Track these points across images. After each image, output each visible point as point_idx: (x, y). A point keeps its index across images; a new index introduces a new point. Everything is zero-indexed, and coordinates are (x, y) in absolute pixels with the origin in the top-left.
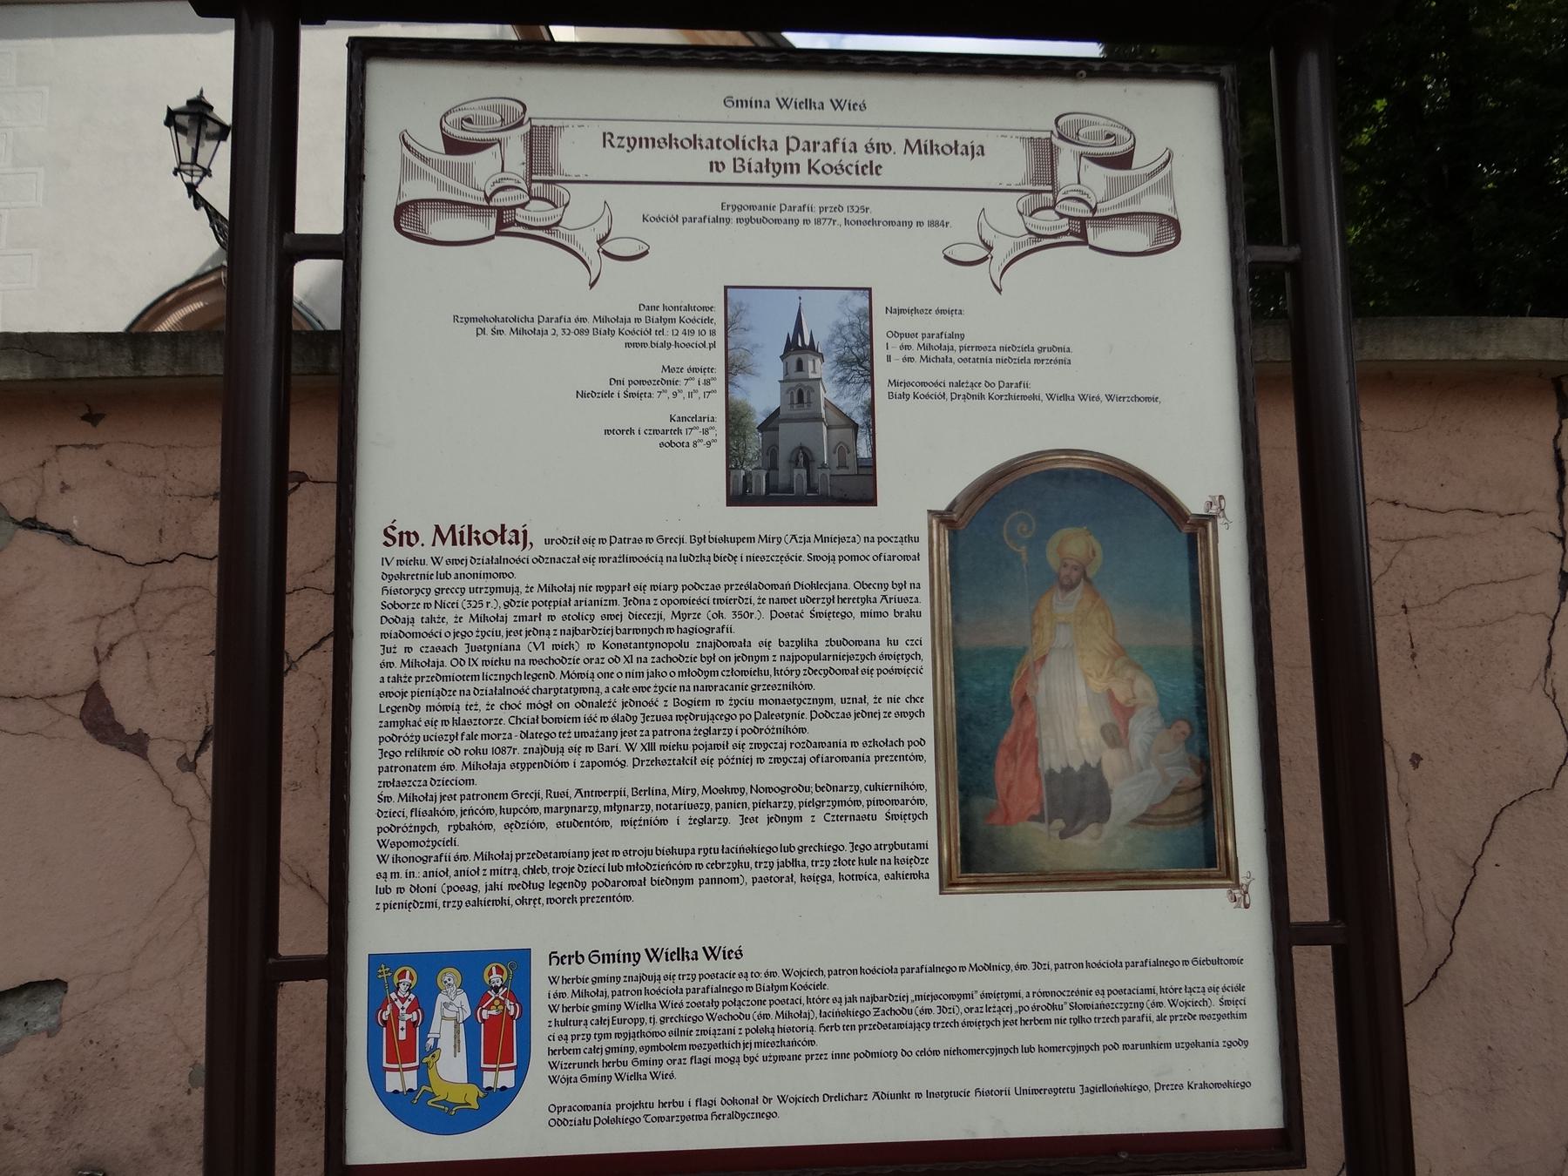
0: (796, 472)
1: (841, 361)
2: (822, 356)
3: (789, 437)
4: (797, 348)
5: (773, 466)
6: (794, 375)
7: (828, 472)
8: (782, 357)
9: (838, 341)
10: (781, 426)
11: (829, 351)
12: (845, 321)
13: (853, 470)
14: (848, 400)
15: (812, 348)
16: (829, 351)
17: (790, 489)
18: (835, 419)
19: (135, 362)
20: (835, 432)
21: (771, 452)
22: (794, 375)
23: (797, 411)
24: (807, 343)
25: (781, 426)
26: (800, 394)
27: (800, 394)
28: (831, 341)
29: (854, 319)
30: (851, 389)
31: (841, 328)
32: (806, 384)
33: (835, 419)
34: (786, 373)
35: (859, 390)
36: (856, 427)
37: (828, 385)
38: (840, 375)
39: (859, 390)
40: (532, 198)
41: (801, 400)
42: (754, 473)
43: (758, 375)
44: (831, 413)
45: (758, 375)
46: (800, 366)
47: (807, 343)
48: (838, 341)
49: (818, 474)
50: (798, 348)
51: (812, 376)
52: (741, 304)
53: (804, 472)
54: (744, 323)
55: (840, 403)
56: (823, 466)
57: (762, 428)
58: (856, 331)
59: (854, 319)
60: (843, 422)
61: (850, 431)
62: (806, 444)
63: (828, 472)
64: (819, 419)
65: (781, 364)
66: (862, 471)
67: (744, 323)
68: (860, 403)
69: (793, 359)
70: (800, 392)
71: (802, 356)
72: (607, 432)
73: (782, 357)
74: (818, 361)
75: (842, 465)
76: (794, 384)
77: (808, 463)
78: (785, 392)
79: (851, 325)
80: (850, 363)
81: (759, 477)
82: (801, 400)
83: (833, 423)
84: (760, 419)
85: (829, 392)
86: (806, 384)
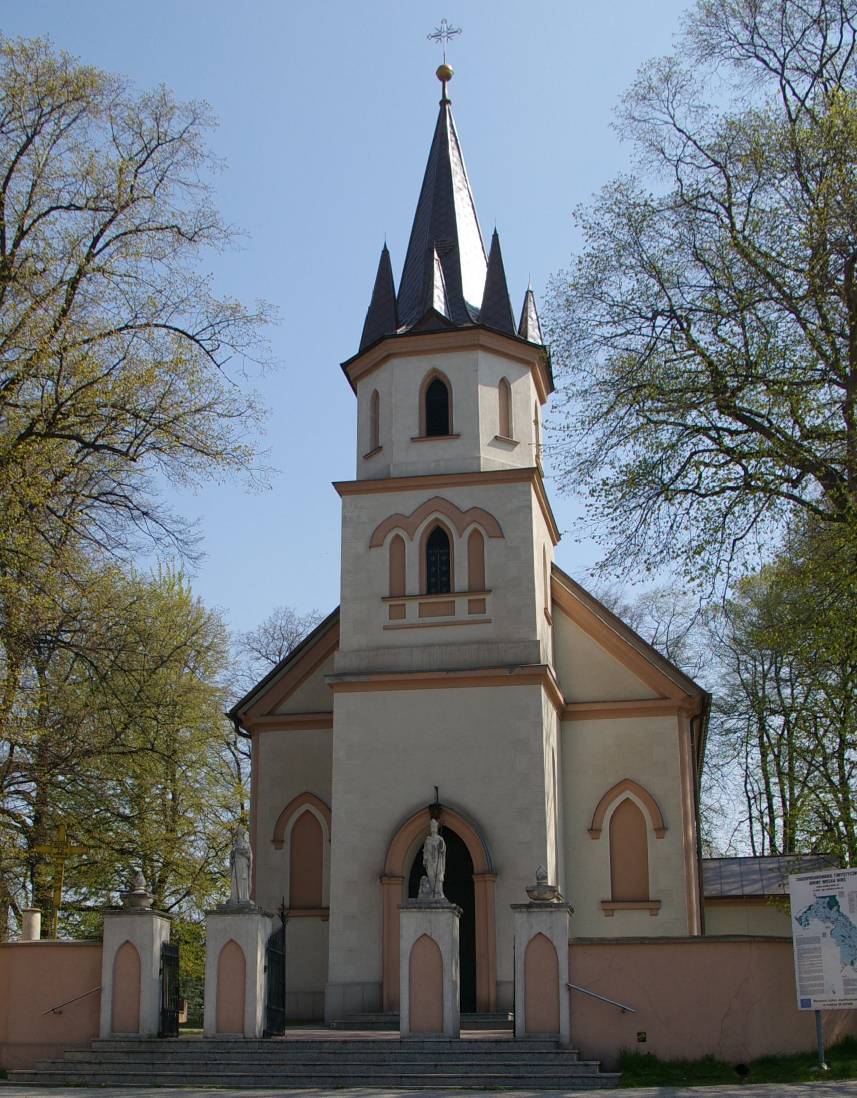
0: (411, 925)
1: (635, 387)
2: (541, 363)
3: (383, 759)
4: (422, 326)
5: (304, 900)
6: (411, 454)
7: (558, 928)
8: (354, 370)
9: (623, 285)
10: (344, 704)
11: (575, 334)
12: (659, 187)
13: (676, 916)
14: (666, 576)
15: (496, 322)
16: (575, 334)
17: (379, 1009)
18: (600, 671)
19: (853, 777)
20: (597, 733)
21: (294, 825)
22: (411, 454)
23: (425, 634)
24: (474, 293)
25: (344, 704)
26: (438, 543)
27: (438, 543)
28: (590, 288)
29: (703, 177)
30: (679, 521)
31: (637, 219)
32: (463, 497)
33: (600, 671)
34: (371, 448)
35: (717, 528)
36: (698, 708)
37: (569, 507)
38: (627, 454)
39: (717, 528)
40: (159, 144)
41: (438, 579)
42: (215, 933)
43: (237, 458)
44: (585, 645)
45: (237, 458)
46: (438, 412)
47: (474, 293)
48: (623, 285)
49: (512, 935)
50: (427, 324)
51: (493, 459)
52: (161, 110)
53: (446, 925)
54: (178, 204)
55: (627, 591)
56: (538, 900)
57: (250, 715)
58: (712, 236)
59: (703, 177)
60: (633, 683)
61: (669, 728)
62: (450, 793)
63: (558, 928)
64: (524, 670)
65: (345, 404)
66: (725, 922)
67: (178, 204)
68: (722, 590)
69: (405, 378)
70: (435, 539)
71: (451, 365)
72: (436, 788)
73: (354, 370)
74: (525, 386)
75: (631, 894)
76: (406, 502)
77: (463, 886)
78: (365, 541)
79: (687, 204)
80: (675, 397)
81: (234, 950)
82: (438, 579)
83: (587, 688)
84: (242, 671)
85: (568, 538)
86: (463, 497)
